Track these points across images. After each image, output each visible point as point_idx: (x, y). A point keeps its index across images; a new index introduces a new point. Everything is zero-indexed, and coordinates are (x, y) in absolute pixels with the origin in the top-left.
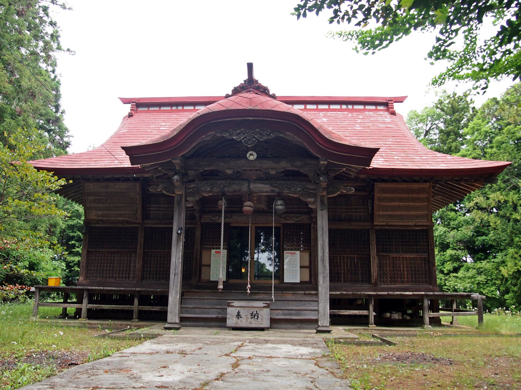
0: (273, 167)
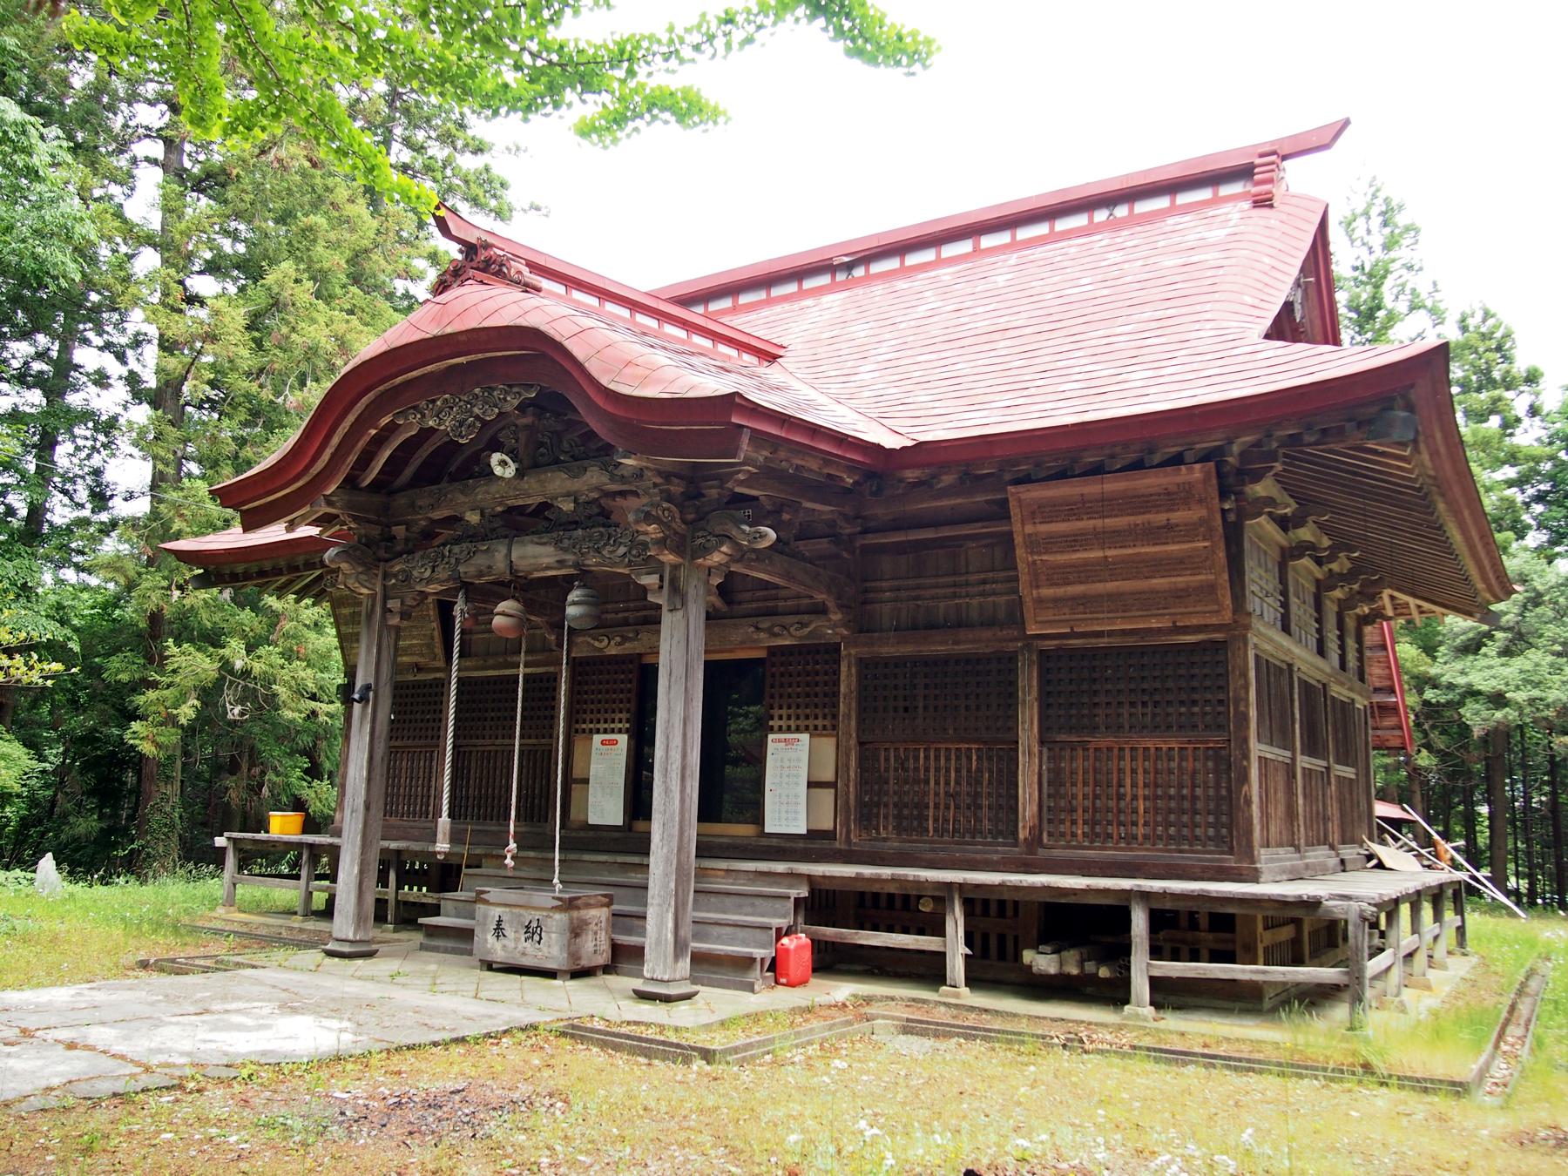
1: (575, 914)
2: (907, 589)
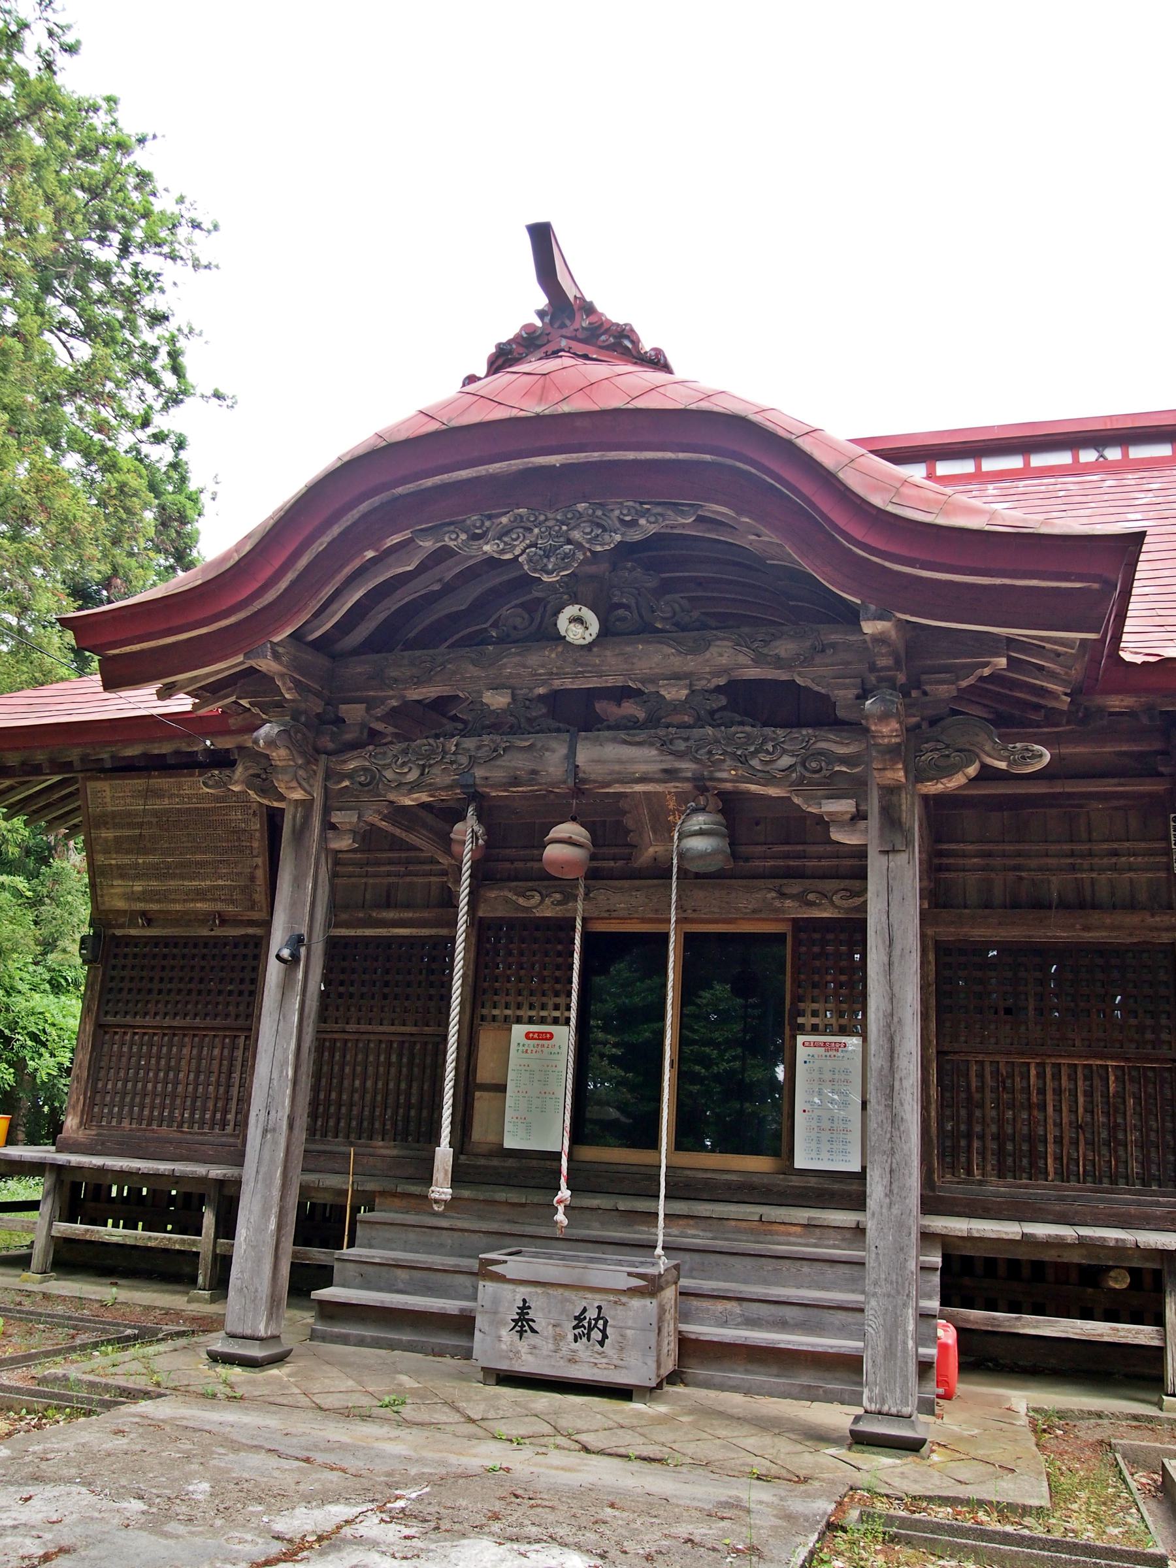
0: (667, 668)
2: (1004, 855)
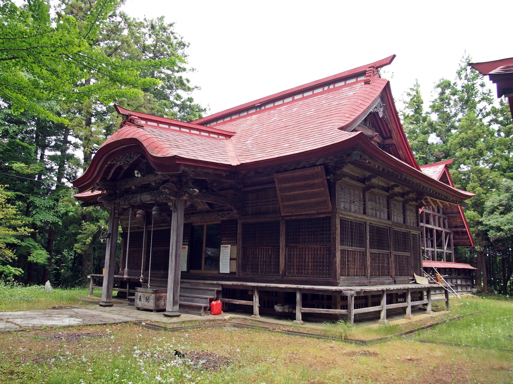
1: (158, 294)
